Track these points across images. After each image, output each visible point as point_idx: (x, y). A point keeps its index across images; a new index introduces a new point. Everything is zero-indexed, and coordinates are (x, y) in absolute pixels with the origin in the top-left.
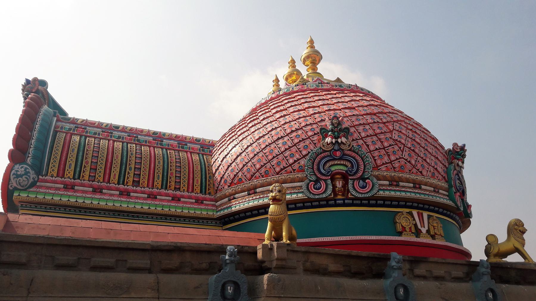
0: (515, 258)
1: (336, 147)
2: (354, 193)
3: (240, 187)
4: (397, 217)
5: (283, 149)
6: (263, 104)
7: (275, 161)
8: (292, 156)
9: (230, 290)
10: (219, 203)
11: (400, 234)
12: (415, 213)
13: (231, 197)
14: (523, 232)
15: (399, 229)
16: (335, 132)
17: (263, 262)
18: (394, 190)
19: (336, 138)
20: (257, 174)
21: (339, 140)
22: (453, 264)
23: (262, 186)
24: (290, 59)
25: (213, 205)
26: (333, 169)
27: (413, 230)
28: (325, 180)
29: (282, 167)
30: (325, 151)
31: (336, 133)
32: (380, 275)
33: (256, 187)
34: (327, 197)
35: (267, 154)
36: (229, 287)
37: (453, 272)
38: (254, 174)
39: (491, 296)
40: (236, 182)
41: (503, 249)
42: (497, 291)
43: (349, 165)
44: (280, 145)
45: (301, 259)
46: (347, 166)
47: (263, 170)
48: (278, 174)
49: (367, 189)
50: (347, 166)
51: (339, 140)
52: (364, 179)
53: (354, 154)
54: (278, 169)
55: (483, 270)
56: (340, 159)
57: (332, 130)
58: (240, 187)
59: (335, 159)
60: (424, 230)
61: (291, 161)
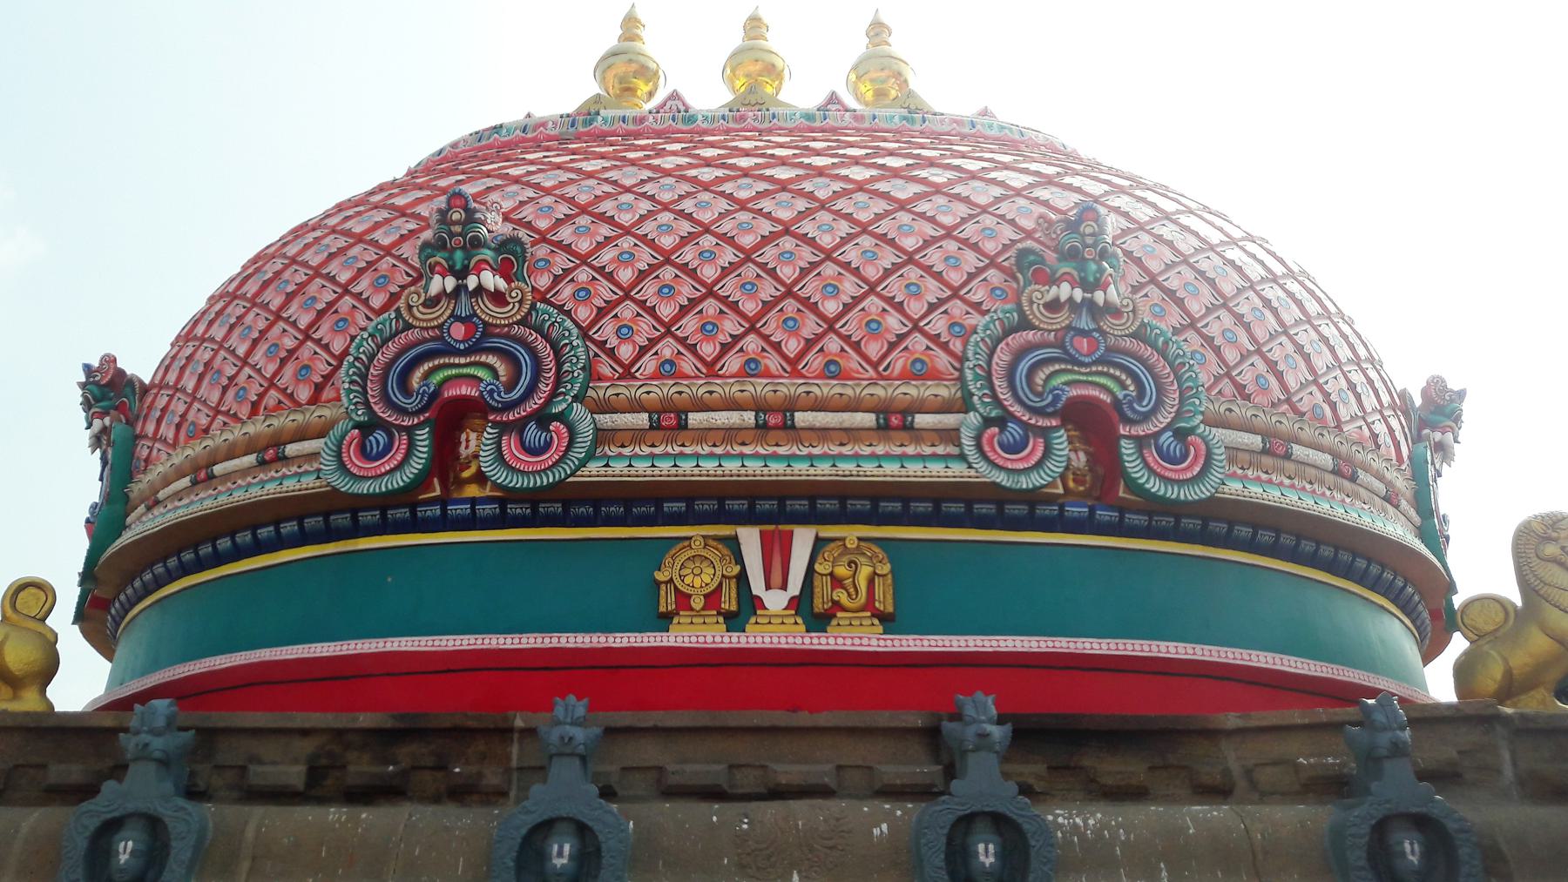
1: (1085, 322)
6: (446, 160)
9: (1413, 852)
11: (664, 621)
12: (750, 538)
15: (667, 602)
16: (453, 250)
18: (920, 457)
21: (1099, 297)
22: (851, 731)
27: (729, 603)
31: (459, 255)
34: (1036, 489)
36: (981, 847)
37: (884, 768)
38: (261, 396)
39: (1414, 859)
43: (502, 369)
45: (208, 732)
46: (1124, 387)
49: (551, 456)
50: (1124, 387)
60: (776, 601)
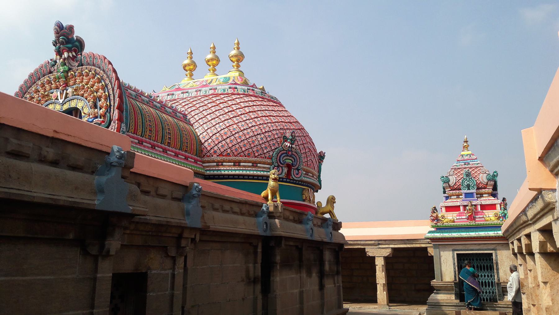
0: (327, 216)
1: (290, 149)
2: (293, 177)
3: (228, 158)
4: (304, 192)
5: (261, 142)
7: (255, 149)
8: (266, 148)
10: (204, 165)
11: (304, 201)
13: (219, 163)
14: (335, 202)
15: (304, 198)
17: (272, 213)
19: (292, 144)
20: (242, 154)
23: (245, 162)
24: (212, 46)
25: (202, 165)
26: (287, 161)
28: (282, 167)
29: (259, 153)
30: (284, 150)
32: (300, 222)
33: (240, 162)
35: (251, 143)
40: (224, 154)
41: (325, 210)
42: (268, 223)
44: (259, 139)
47: (246, 153)
48: (255, 157)
49: (299, 176)
51: (293, 146)
52: (298, 170)
53: (296, 155)
54: (257, 154)
55: (330, 223)
56: (290, 156)
57: (291, 140)
58: (228, 158)
59: (288, 156)
61: (265, 151)
